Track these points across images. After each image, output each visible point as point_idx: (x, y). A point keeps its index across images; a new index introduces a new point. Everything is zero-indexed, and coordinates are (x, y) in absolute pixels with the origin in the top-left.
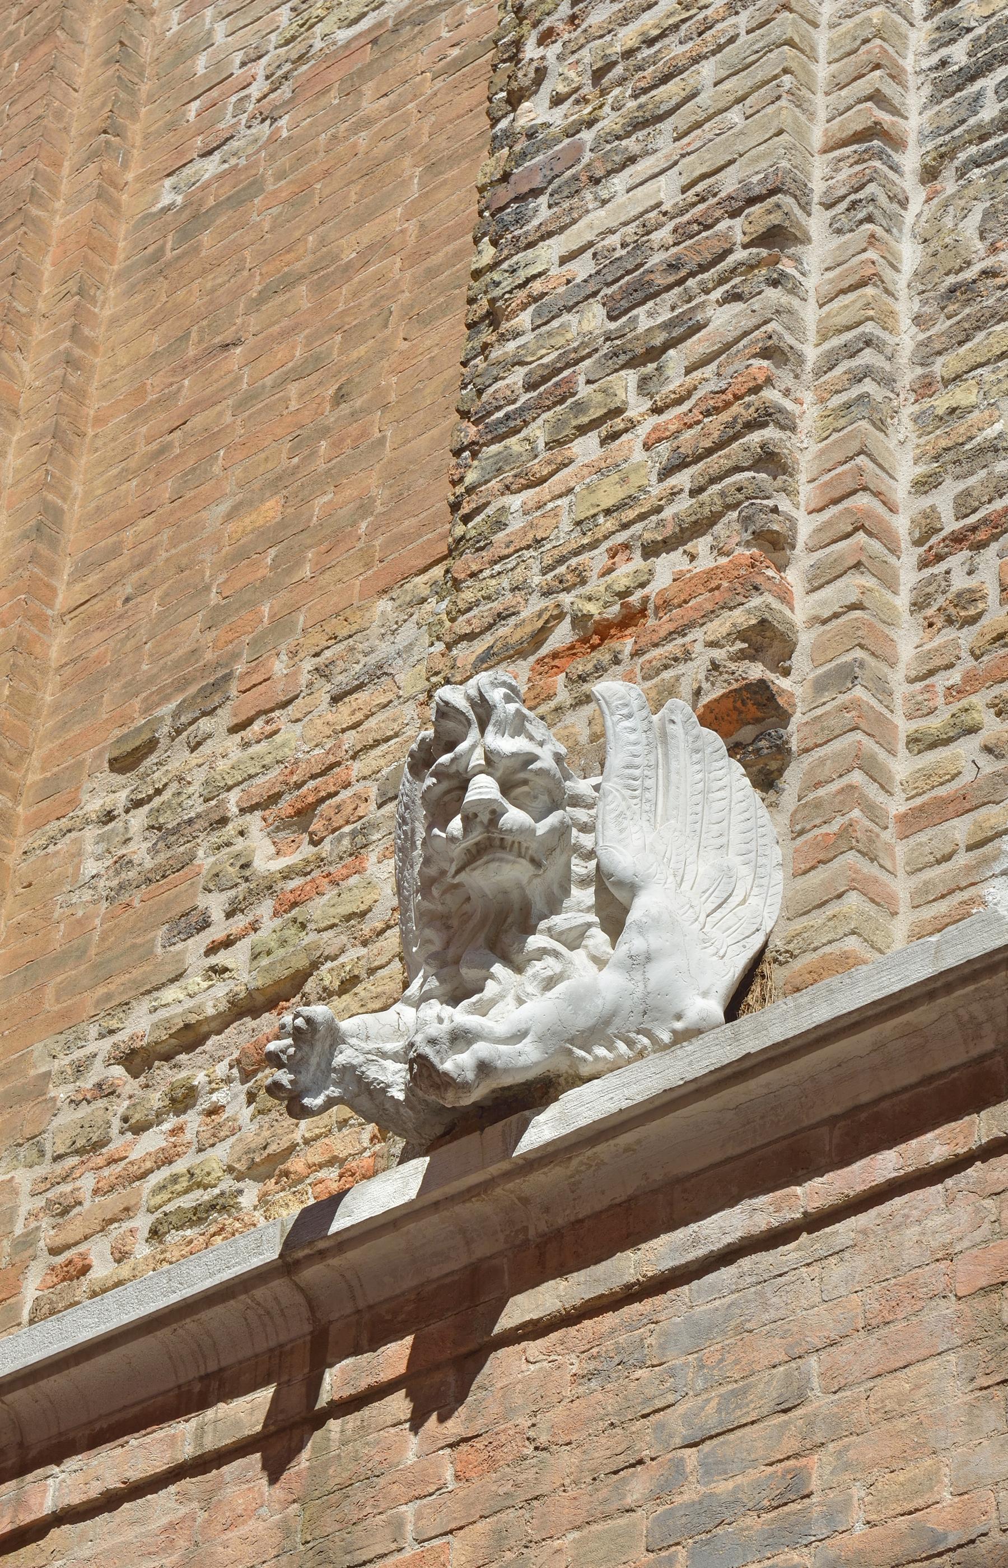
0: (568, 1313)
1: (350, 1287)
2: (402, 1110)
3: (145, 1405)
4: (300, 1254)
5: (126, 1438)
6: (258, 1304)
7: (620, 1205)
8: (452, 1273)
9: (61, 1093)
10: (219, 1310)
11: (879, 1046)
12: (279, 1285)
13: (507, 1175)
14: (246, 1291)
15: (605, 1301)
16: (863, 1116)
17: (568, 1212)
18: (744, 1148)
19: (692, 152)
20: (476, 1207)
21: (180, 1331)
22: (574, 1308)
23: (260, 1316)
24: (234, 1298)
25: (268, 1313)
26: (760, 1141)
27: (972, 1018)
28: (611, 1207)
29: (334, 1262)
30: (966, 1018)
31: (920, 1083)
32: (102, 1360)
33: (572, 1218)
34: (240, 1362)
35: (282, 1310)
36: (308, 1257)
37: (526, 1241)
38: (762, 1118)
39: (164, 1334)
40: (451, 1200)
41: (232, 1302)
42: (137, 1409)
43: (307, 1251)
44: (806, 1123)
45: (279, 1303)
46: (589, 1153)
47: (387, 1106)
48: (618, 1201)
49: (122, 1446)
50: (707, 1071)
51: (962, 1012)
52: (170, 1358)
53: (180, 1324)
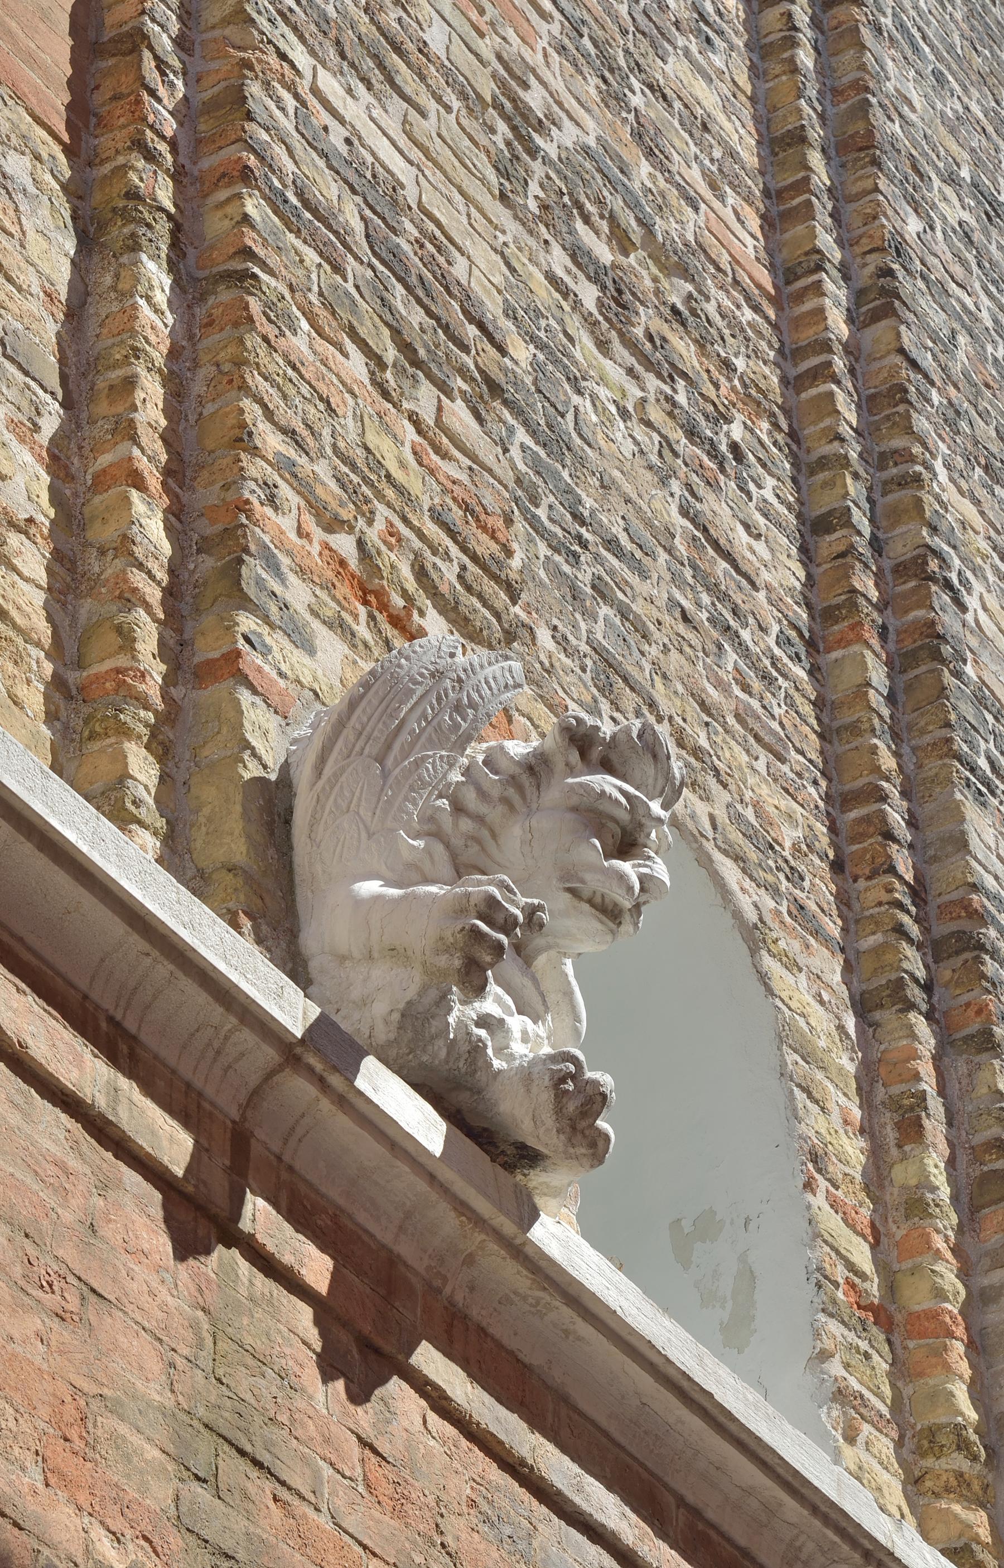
0: (470, 1422)
1: (293, 1129)
2: (440, 1042)
3: (44, 968)
4: (312, 1060)
5: (28, 990)
6: (226, 1038)
7: (518, 1360)
8: (372, 1236)
9: (946, 1223)
10: (202, 997)
11: (748, 1491)
12: (269, 1054)
13: (498, 1235)
14: (242, 1021)
15: (498, 1449)
16: (701, 1526)
17: (483, 1312)
18: (622, 1441)
19: (650, 19)
20: (450, 1222)
21: (148, 961)
22: (478, 1424)
23: (209, 1044)
24: (227, 1010)
25: (218, 1052)
26: (633, 1449)
27: (800, 1549)
28: (511, 1353)
29: (325, 1105)
30: (798, 1544)
31: (738, 1548)
32: (61, 879)
33: (484, 1324)
34: (156, 1057)
35: (230, 1067)
36: (311, 1069)
37: (439, 1291)
38: (646, 1432)
39: (137, 943)
40: (445, 1190)
41: (221, 1010)
42: (35, 962)
43: (319, 1067)
44: (666, 1479)
45: (237, 1060)
46: (557, 1304)
47: (434, 1023)
48: (521, 1356)
49: (18, 990)
50: (683, 1368)
51: (802, 1538)
52: (102, 960)
53: (161, 958)
